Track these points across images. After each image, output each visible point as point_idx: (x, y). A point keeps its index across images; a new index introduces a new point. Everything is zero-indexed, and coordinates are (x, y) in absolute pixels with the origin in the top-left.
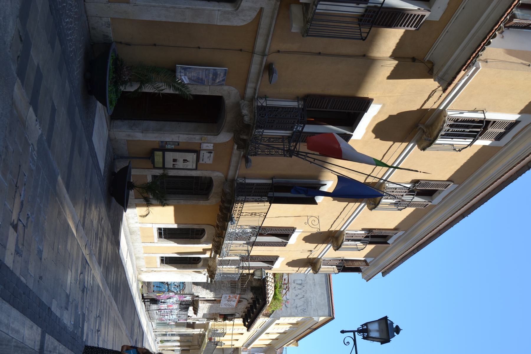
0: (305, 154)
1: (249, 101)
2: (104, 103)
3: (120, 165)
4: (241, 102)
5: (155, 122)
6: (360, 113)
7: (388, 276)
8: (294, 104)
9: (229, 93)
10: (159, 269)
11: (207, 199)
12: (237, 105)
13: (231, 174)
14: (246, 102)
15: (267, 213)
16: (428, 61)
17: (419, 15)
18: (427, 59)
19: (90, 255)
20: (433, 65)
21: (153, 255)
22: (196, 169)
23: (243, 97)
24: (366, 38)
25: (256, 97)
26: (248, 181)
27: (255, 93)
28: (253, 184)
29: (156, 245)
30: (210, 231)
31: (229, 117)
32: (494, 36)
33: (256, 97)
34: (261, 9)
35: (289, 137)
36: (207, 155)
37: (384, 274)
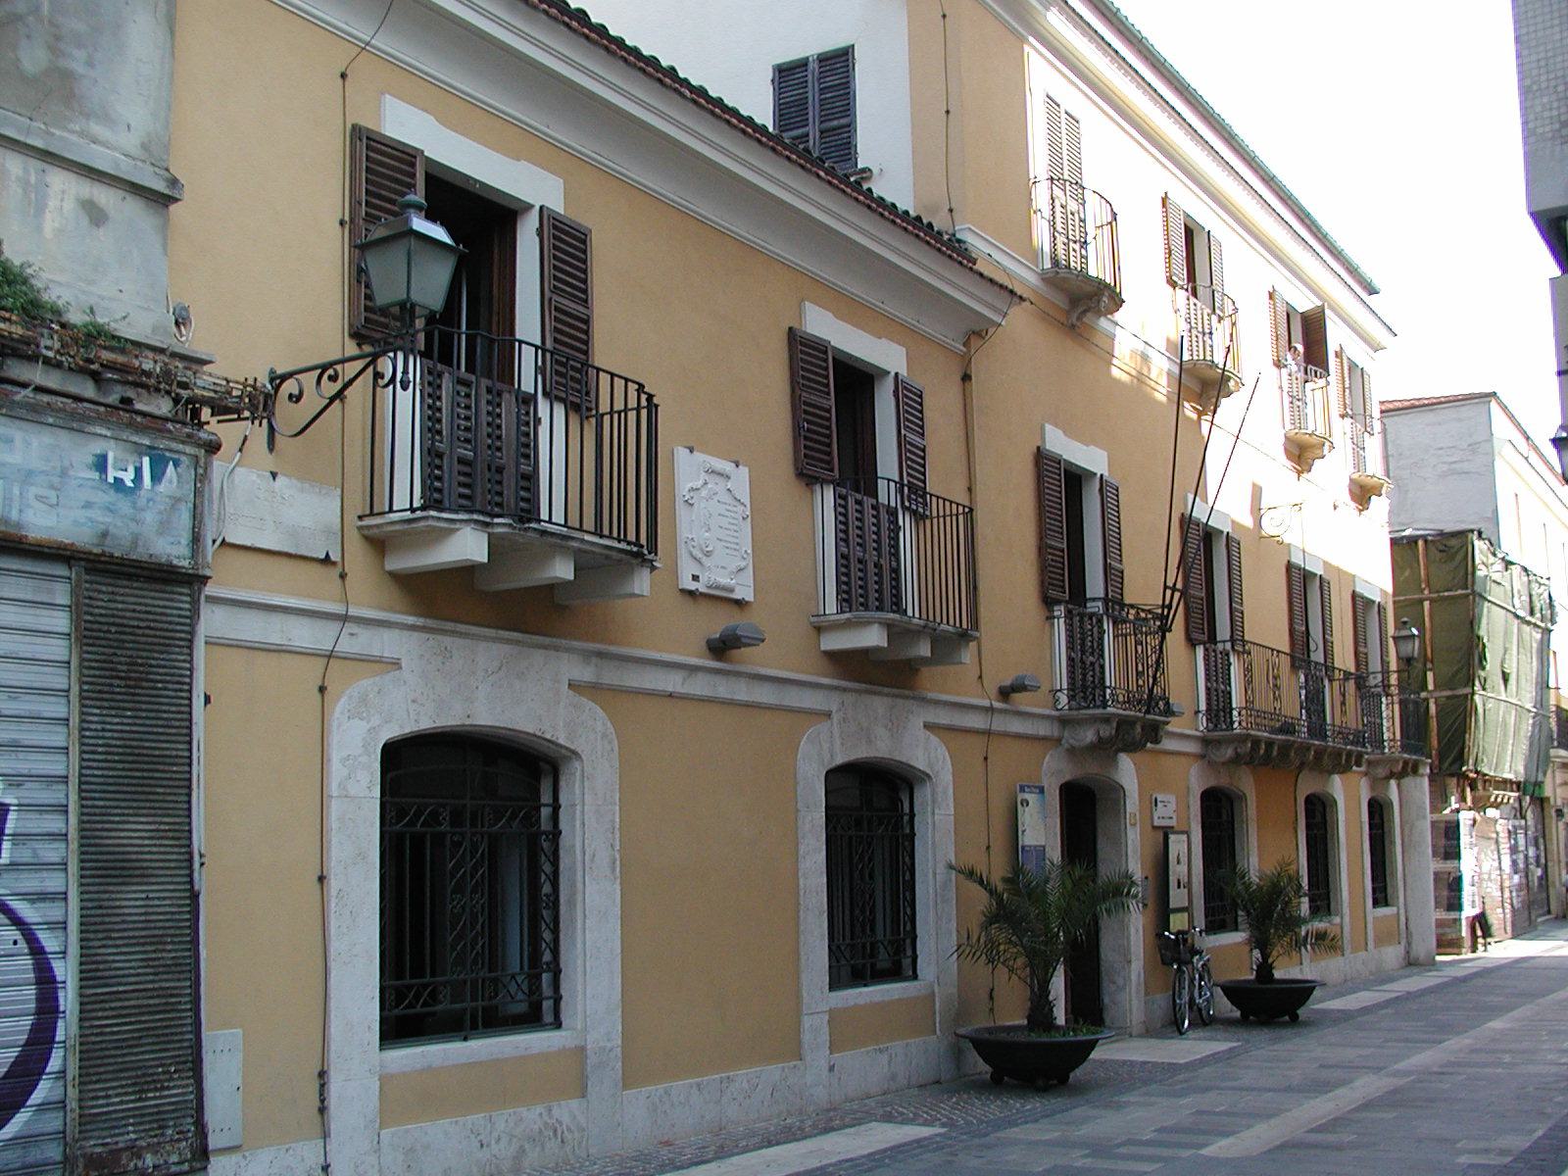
0: (1169, 592)
1: (1064, 728)
2: (1091, 1045)
3: (1224, 1006)
4: (1066, 746)
5: (1101, 934)
6: (430, 179)
7: (1377, 283)
8: (1060, 626)
9: (1054, 771)
10: (1402, 911)
11: (1242, 798)
12: (1072, 752)
13: (1192, 747)
14: (1066, 734)
15: (1273, 650)
16: (964, 345)
17: (555, 237)
18: (962, 348)
19: (1220, 1148)
20: (974, 332)
21: (1370, 926)
22: (1187, 833)
23: (1059, 740)
24: (637, 383)
25: (1054, 713)
26: (1203, 707)
27: (1048, 717)
28: (1208, 689)
29: (1347, 919)
30: (1307, 785)
31: (1090, 769)
32: (870, 190)
33: (1054, 713)
34: (927, 726)
35: (1115, 623)
36: (1160, 811)
37: (1372, 291)
